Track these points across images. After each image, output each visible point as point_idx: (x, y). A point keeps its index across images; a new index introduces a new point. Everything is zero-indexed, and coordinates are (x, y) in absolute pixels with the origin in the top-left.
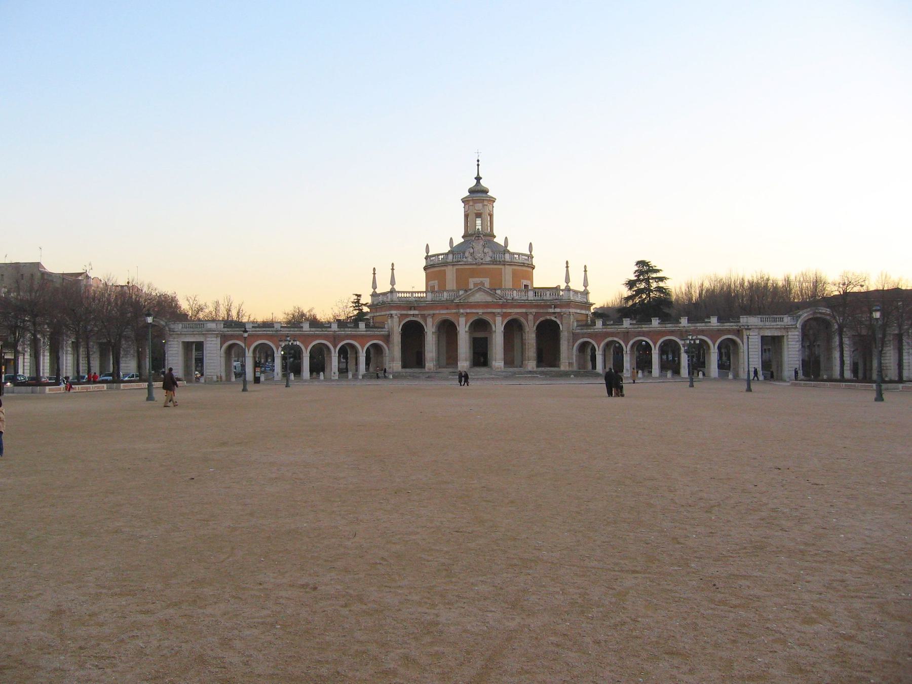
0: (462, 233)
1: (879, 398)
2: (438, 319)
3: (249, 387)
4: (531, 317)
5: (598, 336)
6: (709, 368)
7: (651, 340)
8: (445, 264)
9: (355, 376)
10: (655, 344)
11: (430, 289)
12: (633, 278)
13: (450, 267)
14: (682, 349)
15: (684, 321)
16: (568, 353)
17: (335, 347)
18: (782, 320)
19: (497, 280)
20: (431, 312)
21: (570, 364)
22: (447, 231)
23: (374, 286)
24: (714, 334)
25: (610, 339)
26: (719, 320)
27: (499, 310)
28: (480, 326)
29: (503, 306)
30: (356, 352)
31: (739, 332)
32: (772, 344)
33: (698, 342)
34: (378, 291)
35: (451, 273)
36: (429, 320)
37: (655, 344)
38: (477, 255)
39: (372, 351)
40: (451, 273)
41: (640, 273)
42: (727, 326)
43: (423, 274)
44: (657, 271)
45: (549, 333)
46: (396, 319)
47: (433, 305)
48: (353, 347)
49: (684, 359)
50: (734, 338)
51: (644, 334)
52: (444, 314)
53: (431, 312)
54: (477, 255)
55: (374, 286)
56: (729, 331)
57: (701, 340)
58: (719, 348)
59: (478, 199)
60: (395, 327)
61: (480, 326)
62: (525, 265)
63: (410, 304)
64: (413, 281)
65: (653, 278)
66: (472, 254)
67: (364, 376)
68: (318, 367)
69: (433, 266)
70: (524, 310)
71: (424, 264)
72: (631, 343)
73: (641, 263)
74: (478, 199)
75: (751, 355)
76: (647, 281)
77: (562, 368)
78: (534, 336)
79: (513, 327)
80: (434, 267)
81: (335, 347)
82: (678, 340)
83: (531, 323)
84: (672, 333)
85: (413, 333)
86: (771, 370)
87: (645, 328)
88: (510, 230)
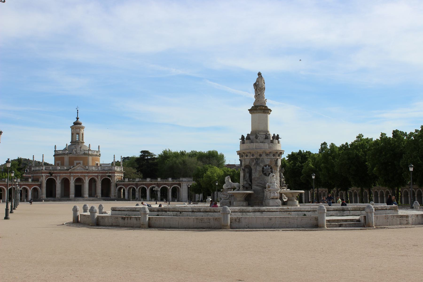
2: (63, 178)
4: (99, 177)
22: (64, 141)
27: (87, 174)
29: (88, 173)
36: (58, 178)
46: (44, 177)
50: (178, 186)
53: (59, 174)
70: (96, 174)
78: (100, 184)
79: (92, 181)
83: (99, 179)
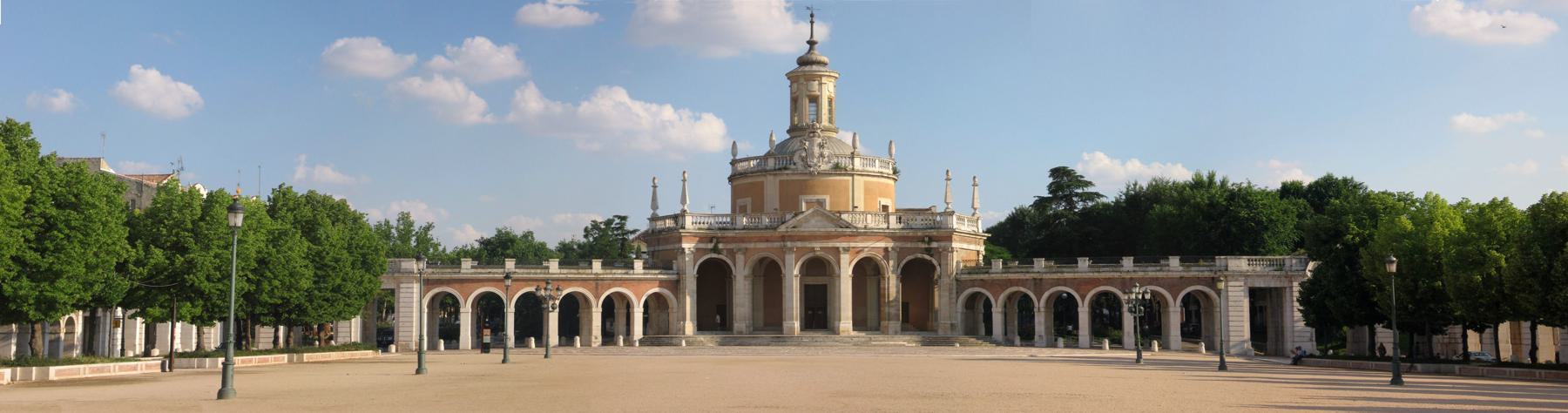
0: (787, 126)
3: (510, 357)
5: (998, 286)
6: (1168, 336)
7: (1170, 292)
8: (761, 171)
9: (629, 341)
10: (1083, 298)
11: (737, 209)
12: (1046, 194)
13: (770, 178)
14: (1125, 308)
15: (554, 266)
17: (597, 297)
18: (503, 265)
20: (845, 245)
21: (70, 322)
23: (655, 206)
24: (1174, 285)
25: (1014, 289)
26: (604, 265)
30: (629, 307)
31: (1212, 282)
32: (1263, 302)
33: (1148, 296)
34: (660, 213)
36: (740, 258)
37: (1083, 298)
39: (652, 304)
40: (771, 186)
41: (1054, 188)
42: (1194, 272)
43: (727, 189)
44: (1089, 184)
48: (622, 296)
49: (553, 320)
51: (1065, 282)
52: (761, 248)
55: (655, 206)
56: (1198, 281)
57: (1154, 293)
58: (646, 305)
65: (1077, 195)
66: (803, 159)
67: (642, 342)
69: (744, 174)
71: (729, 173)
72: (1046, 295)
73: (1057, 172)
75: (1237, 320)
76: (1068, 199)
77: (941, 333)
81: (597, 297)
82: (1119, 293)
84: (1109, 281)
86: (1265, 337)
87: (584, 273)
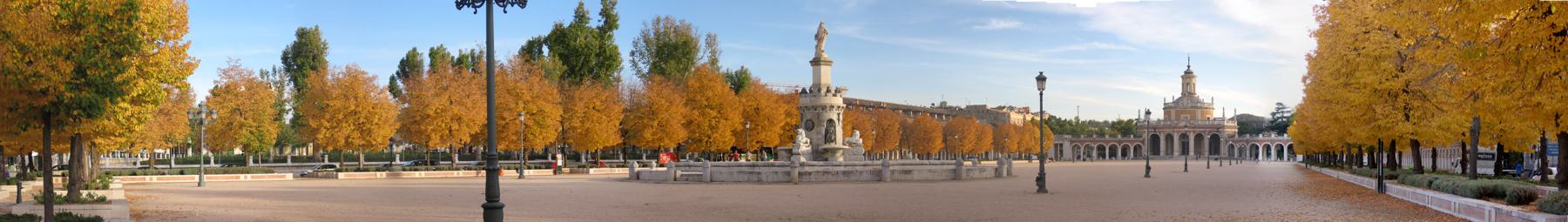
1: (1148, 113)
16: (1224, 149)
19: (1193, 117)
22: (1174, 91)
28: (1184, 136)
35: (1173, 112)
38: (1186, 104)
40: (1173, 112)
45: (1215, 140)
47: (1164, 127)
52: (1168, 131)
54: (1186, 104)
59: (1188, 75)
60: (1146, 136)
61: (1184, 136)
62: (1209, 108)
63: (1157, 126)
64: (1158, 114)
68: (1124, 154)
74: (1188, 75)
79: (1199, 138)
80: (1167, 108)
85: (1155, 140)
88: (1203, 92)
